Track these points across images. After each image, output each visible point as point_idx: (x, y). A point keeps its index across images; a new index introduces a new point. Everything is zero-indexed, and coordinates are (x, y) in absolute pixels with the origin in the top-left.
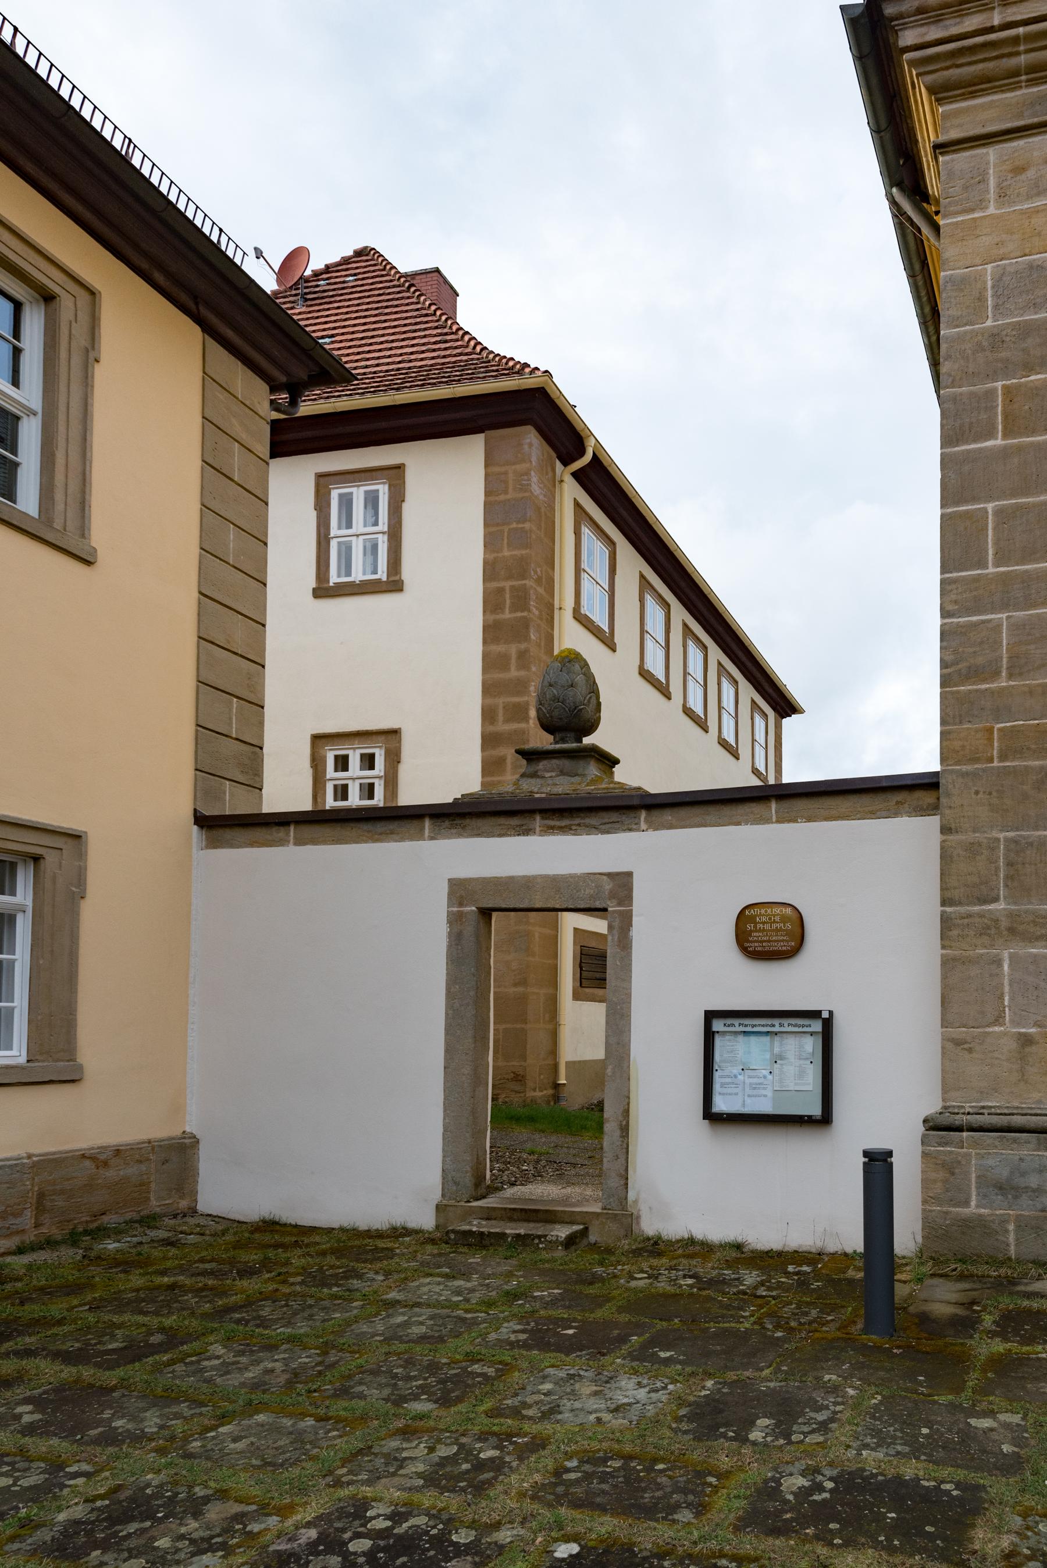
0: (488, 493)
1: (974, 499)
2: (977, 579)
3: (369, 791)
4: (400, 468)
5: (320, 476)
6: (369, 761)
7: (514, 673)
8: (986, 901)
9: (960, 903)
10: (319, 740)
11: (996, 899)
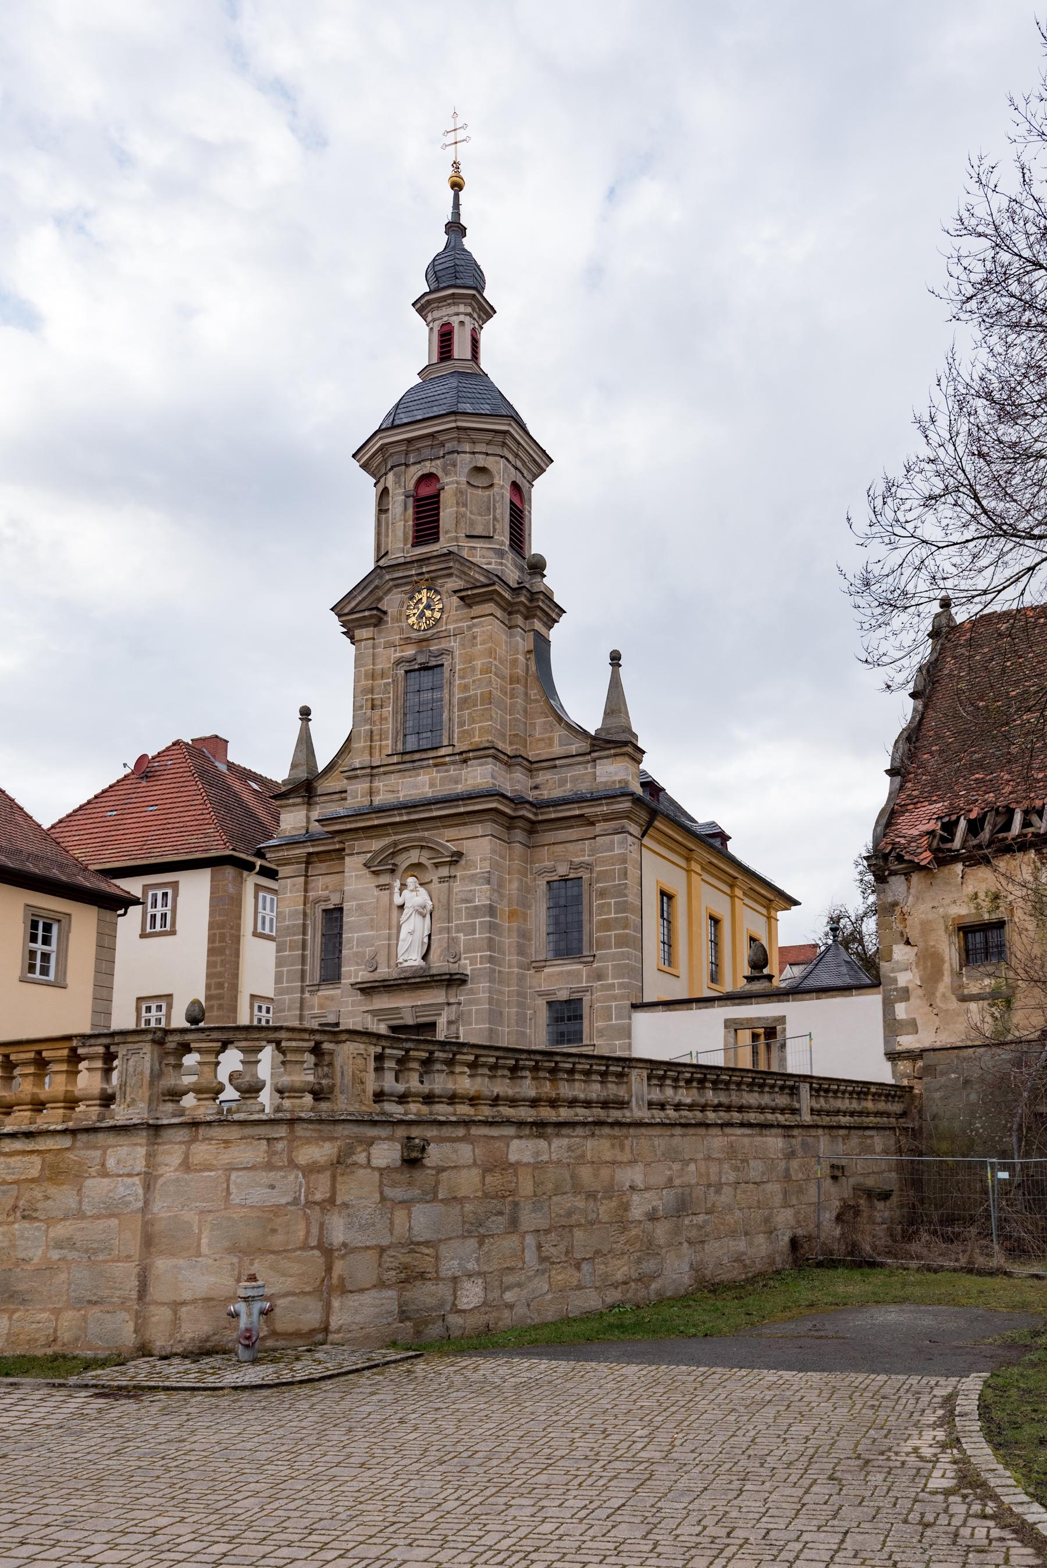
0: (211, 893)
3: (159, 1021)
4: (177, 882)
5: (144, 886)
6: (159, 1008)
7: (219, 969)
10: (139, 1000)
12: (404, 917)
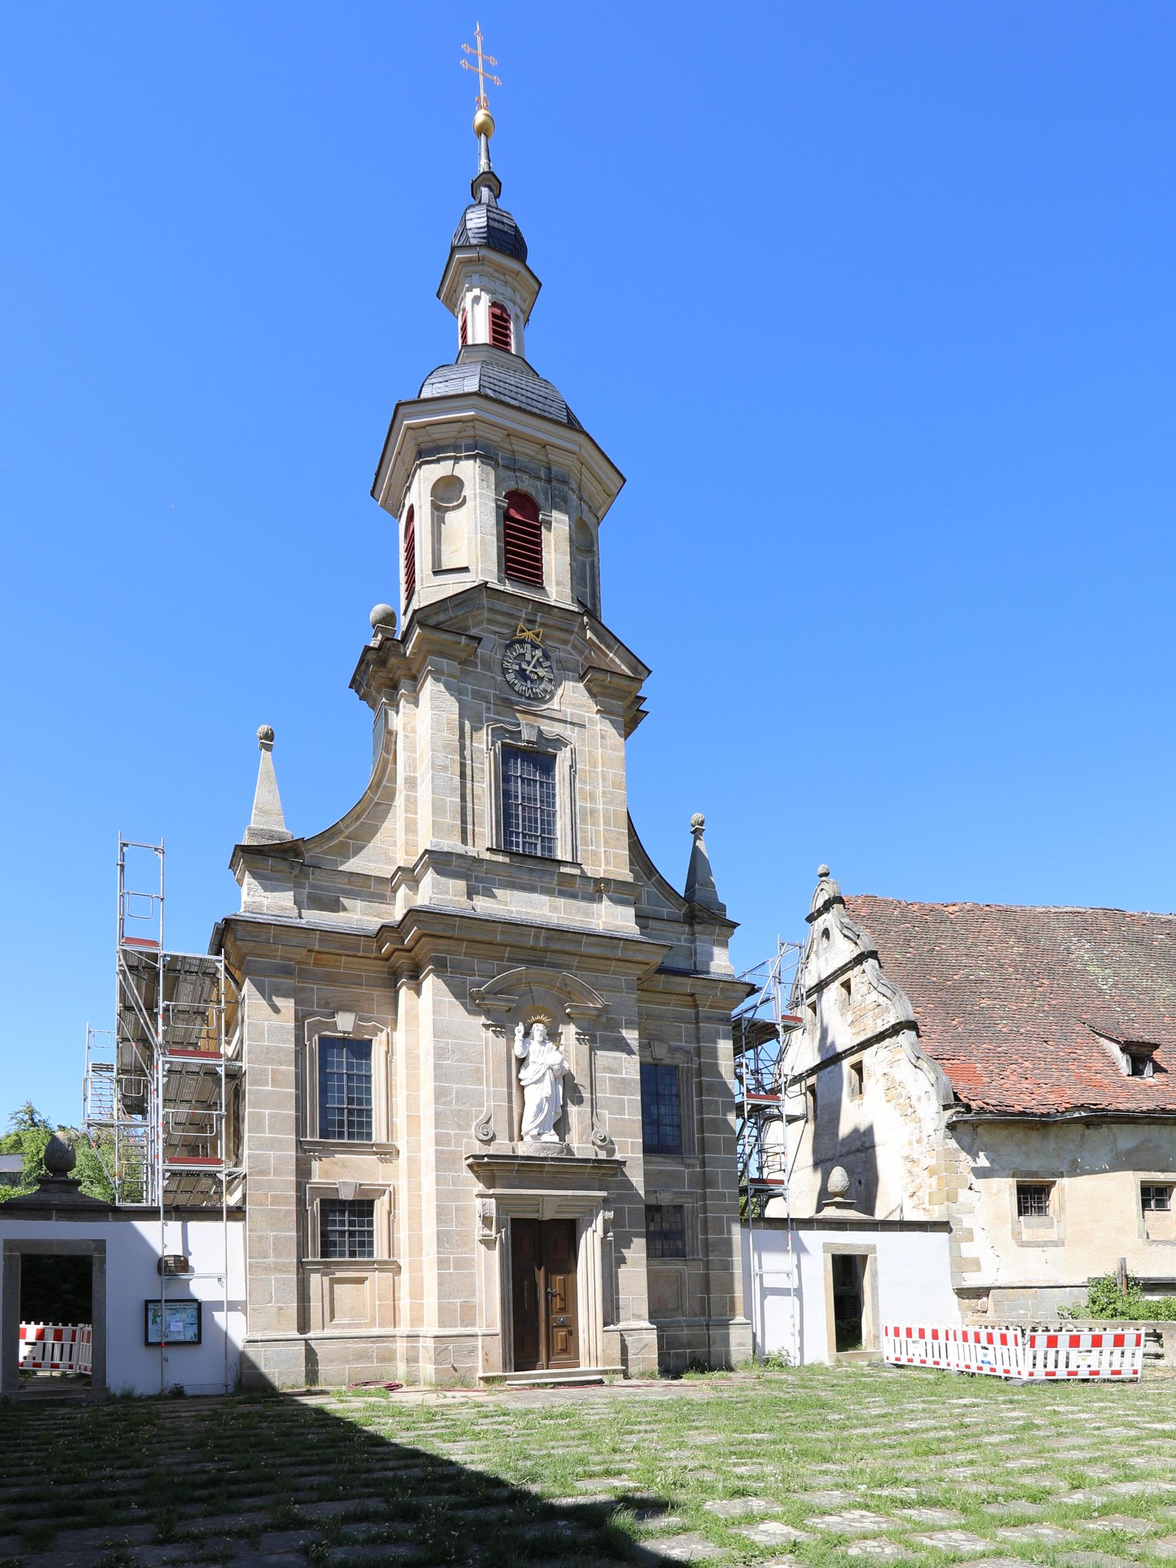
1: (260, 1108)
2: (262, 1137)
8: (264, 1258)
9: (256, 1258)
11: (269, 1257)
12: (526, 1075)
